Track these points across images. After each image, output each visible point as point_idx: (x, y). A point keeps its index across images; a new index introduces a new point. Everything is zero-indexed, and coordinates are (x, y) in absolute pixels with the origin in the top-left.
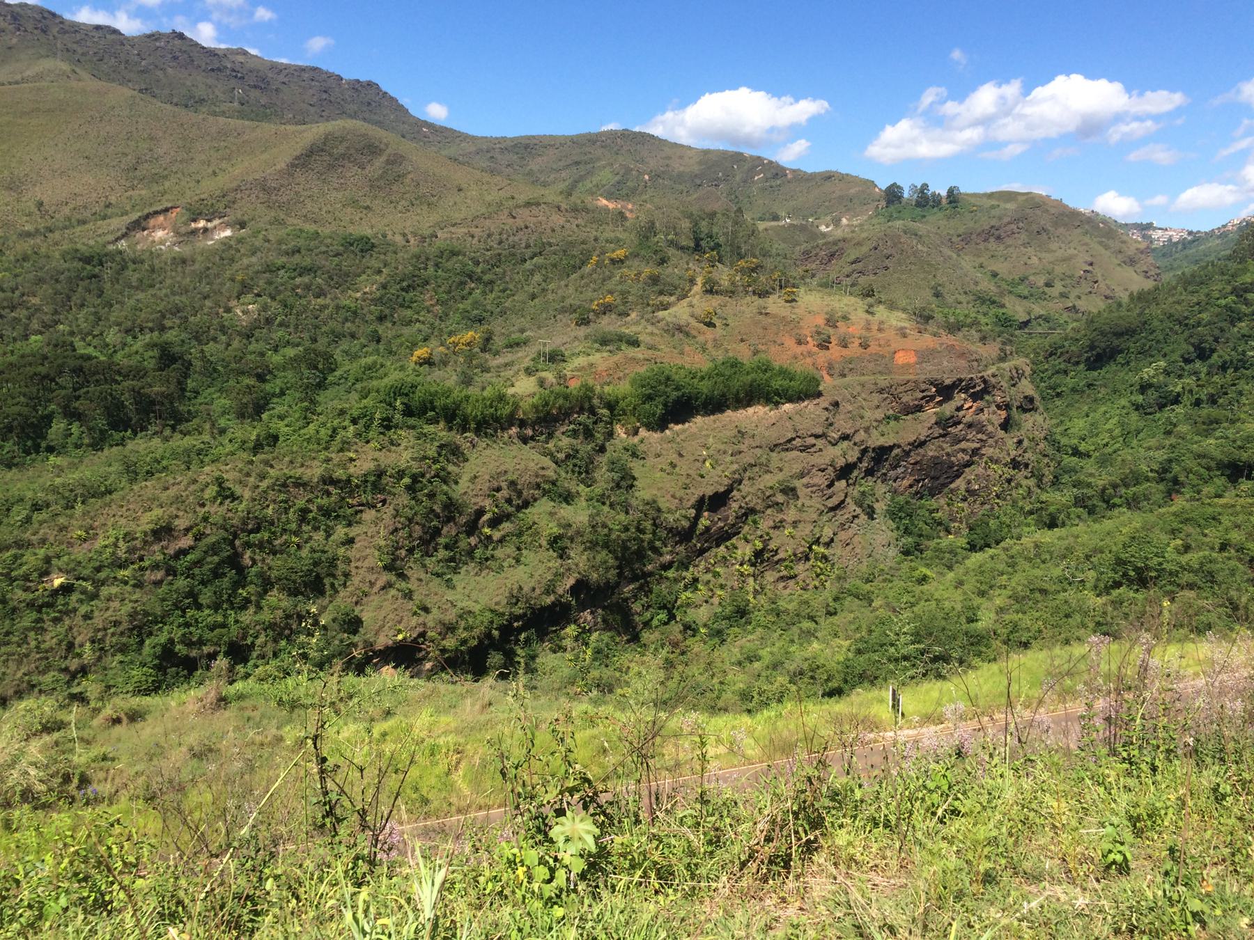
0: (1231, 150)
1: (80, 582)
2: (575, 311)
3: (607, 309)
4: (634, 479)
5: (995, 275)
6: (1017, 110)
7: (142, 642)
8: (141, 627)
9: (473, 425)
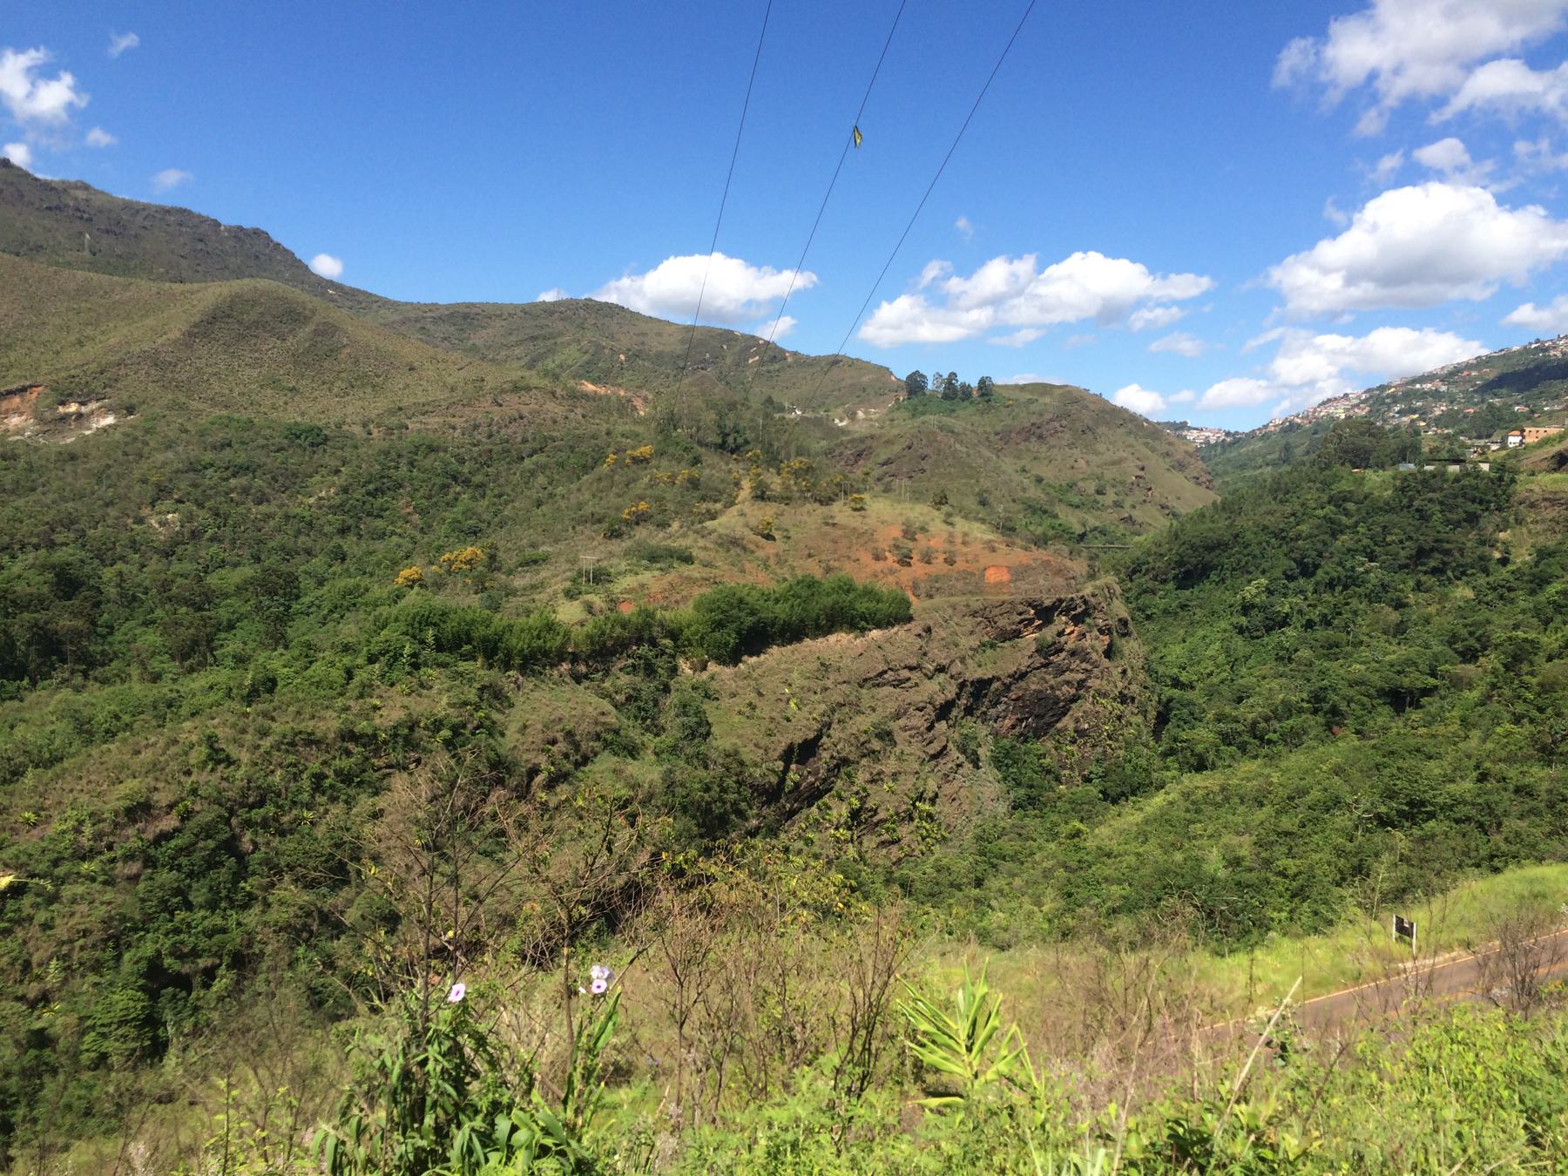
0: (1261, 341)
1: (36, 880)
2: (600, 521)
3: (640, 519)
4: (708, 724)
5: (1039, 480)
6: (1031, 288)
7: (118, 958)
8: (117, 937)
9: (518, 661)
